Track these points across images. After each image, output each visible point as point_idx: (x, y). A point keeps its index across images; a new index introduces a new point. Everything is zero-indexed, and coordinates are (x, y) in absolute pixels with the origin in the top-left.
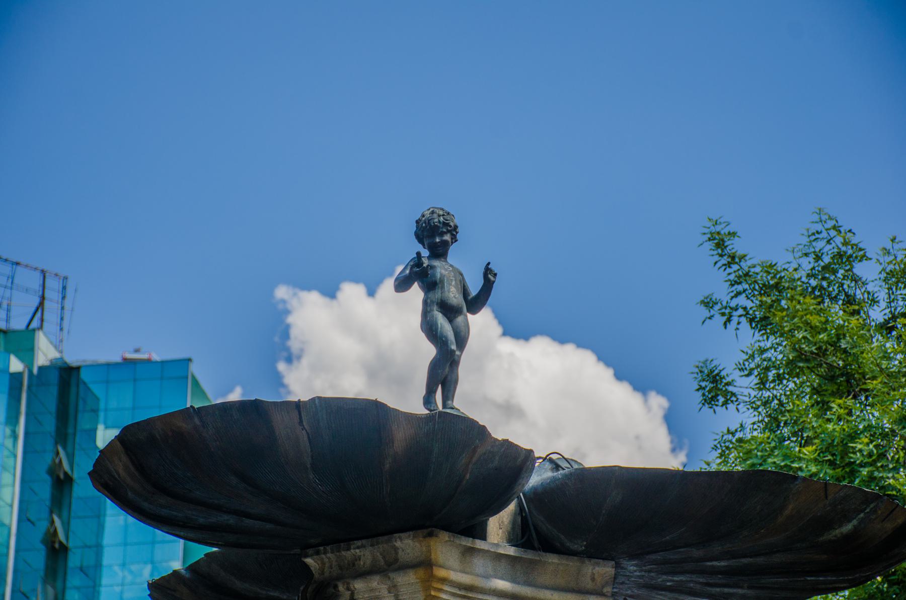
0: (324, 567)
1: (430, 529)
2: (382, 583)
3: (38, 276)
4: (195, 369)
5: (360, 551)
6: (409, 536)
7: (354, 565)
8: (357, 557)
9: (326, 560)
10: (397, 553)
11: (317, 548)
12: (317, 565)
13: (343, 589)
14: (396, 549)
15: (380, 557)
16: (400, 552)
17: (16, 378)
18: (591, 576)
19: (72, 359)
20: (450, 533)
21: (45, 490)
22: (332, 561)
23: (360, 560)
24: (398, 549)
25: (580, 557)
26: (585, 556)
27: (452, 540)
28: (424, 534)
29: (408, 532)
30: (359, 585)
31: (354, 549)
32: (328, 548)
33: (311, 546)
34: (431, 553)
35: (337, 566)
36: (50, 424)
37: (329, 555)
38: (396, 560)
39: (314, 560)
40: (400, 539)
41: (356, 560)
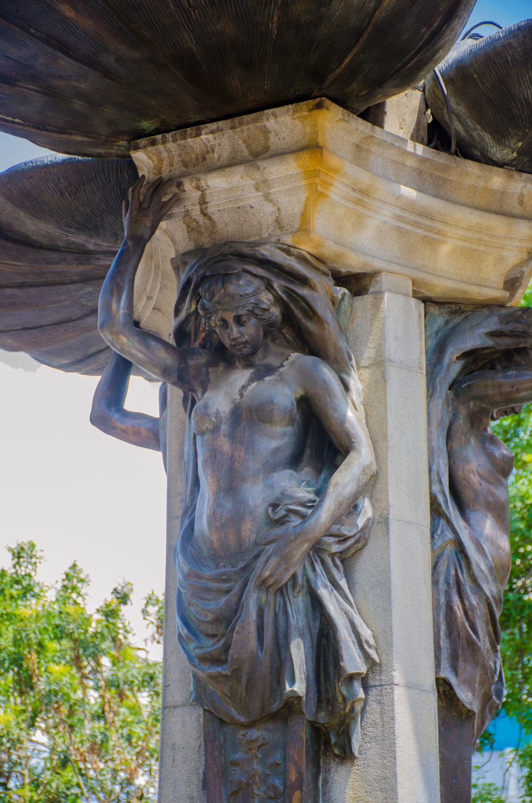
0: (162, 164)
1: (319, 99)
2: (248, 176)
5: (215, 138)
6: (288, 111)
7: (204, 159)
8: (209, 148)
9: (165, 155)
10: (267, 139)
11: (152, 137)
12: (151, 162)
13: (191, 187)
14: (266, 132)
15: (243, 147)
16: (272, 137)
18: (519, 199)
20: (344, 110)
22: (173, 156)
23: (213, 151)
24: (270, 132)
25: (508, 169)
26: (514, 169)
27: (346, 119)
28: (310, 107)
29: (286, 106)
31: (206, 134)
32: (169, 136)
33: (142, 134)
34: (318, 135)
35: (180, 162)
38: (267, 148)
39: (147, 154)
40: (274, 116)
41: (208, 152)
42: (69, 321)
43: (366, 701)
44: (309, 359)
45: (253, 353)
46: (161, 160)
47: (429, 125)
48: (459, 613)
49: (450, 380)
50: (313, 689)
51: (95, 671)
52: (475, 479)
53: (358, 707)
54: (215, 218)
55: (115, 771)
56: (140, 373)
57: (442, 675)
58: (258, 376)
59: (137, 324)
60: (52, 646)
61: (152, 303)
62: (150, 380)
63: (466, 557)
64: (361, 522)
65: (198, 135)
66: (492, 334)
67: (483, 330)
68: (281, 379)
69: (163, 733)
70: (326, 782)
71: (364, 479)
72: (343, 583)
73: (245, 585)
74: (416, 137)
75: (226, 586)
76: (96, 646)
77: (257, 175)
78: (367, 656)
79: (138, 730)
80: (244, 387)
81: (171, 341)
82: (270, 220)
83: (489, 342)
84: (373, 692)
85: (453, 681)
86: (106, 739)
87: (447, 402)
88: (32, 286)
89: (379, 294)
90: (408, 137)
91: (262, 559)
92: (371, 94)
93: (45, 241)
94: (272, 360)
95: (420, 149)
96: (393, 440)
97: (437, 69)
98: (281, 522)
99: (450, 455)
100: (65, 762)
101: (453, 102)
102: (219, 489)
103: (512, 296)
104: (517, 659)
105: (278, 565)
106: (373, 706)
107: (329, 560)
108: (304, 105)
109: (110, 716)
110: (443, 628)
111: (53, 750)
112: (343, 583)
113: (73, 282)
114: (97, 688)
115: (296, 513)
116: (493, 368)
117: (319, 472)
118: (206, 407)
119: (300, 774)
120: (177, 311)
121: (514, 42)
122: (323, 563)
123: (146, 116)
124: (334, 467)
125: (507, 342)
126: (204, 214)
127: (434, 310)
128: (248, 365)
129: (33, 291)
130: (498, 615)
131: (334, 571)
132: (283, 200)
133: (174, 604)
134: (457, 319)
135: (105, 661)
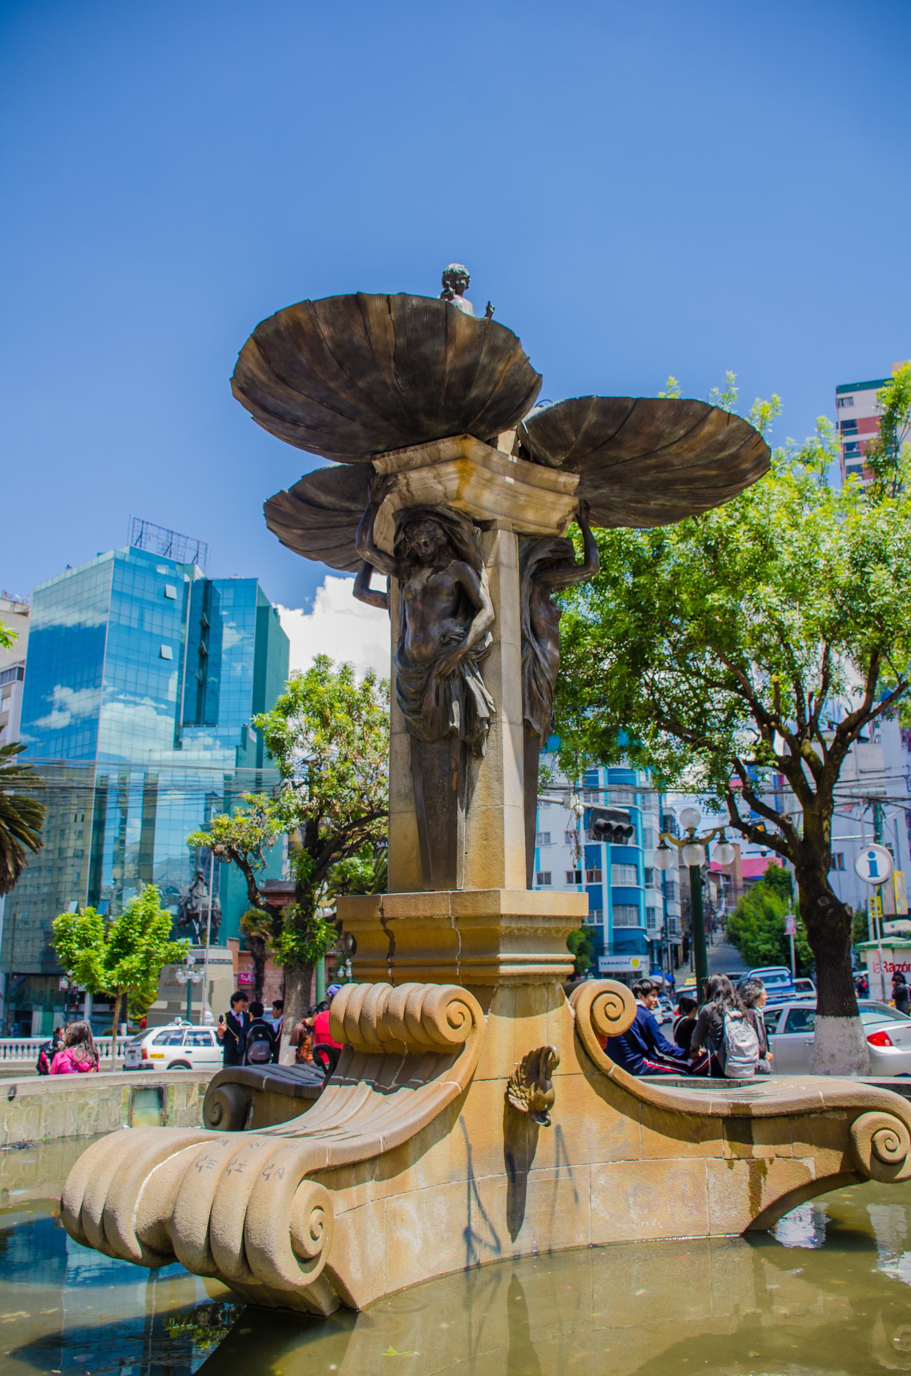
3: (196, 543)
4: (260, 583)
14: (439, 450)
16: (442, 453)
17: (187, 584)
19: (210, 578)
21: (199, 631)
30: (414, 475)
32: (391, 453)
36: (200, 604)
37: (392, 457)
38: (439, 458)
42: (342, 545)
43: (489, 730)
44: (461, 563)
45: (433, 560)
46: (387, 465)
47: (520, 448)
48: (535, 687)
49: (531, 573)
50: (463, 725)
51: (359, 717)
52: (543, 622)
53: (485, 733)
54: (414, 493)
55: (370, 765)
56: (377, 571)
57: (526, 717)
58: (436, 571)
59: (375, 546)
60: (337, 705)
61: (383, 536)
62: (382, 574)
63: (538, 660)
64: (487, 644)
65: (405, 452)
66: (551, 551)
67: (547, 549)
68: (447, 573)
69: (391, 746)
70: (469, 768)
71: (489, 623)
72: (478, 674)
73: (430, 676)
74: (513, 453)
75: (420, 676)
76: (358, 705)
77: (435, 471)
78: (489, 709)
79: (380, 744)
80: (429, 577)
81: (392, 554)
82: (441, 494)
83: (549, 555)
84: (493, 726)
85: (531, 720)
86: (365, 748)
87: (529, 584)
88: (324, 528)
89: (496, 530)
90: (509, 453)
91: (438, 662)
92: (491, 432)
93: (330, 506)
94: (443, 564)
95: (515, 459)
96: (503, 603)
97: (523, 421)
98: (447, 644)
99: (531, 611)
100: (346, 759)
101: (531, 438)
102: (416, 628)
103: (561, 532)
104: (714, 713)
105: (446, 666)
106: (492, 733)
107: (471, 663)
108: (457, 437)
109: (366, 738)
110: (527, 695)
111: (340, 754)
112: (478, 674)
113: (344, 526)
114: (360, 725)
115: (455, 640)
116: (552, 567)
117: (466, 619)
118: (410, 587)
119: (457, 764)
120: (395, 539)
121: (559, 409)
122: (468, 664)
123: (380, 443)
124: (474, 617)
125: (556, 556)
126: (408, 490)
127: (523, 538)
128: (430, 567)
129: (325, 531)
130: (553, 688)
131: (474, 668)
132: (448, 484)
133: (395, 684)
134: (534, 543)
135: (363, 712)
